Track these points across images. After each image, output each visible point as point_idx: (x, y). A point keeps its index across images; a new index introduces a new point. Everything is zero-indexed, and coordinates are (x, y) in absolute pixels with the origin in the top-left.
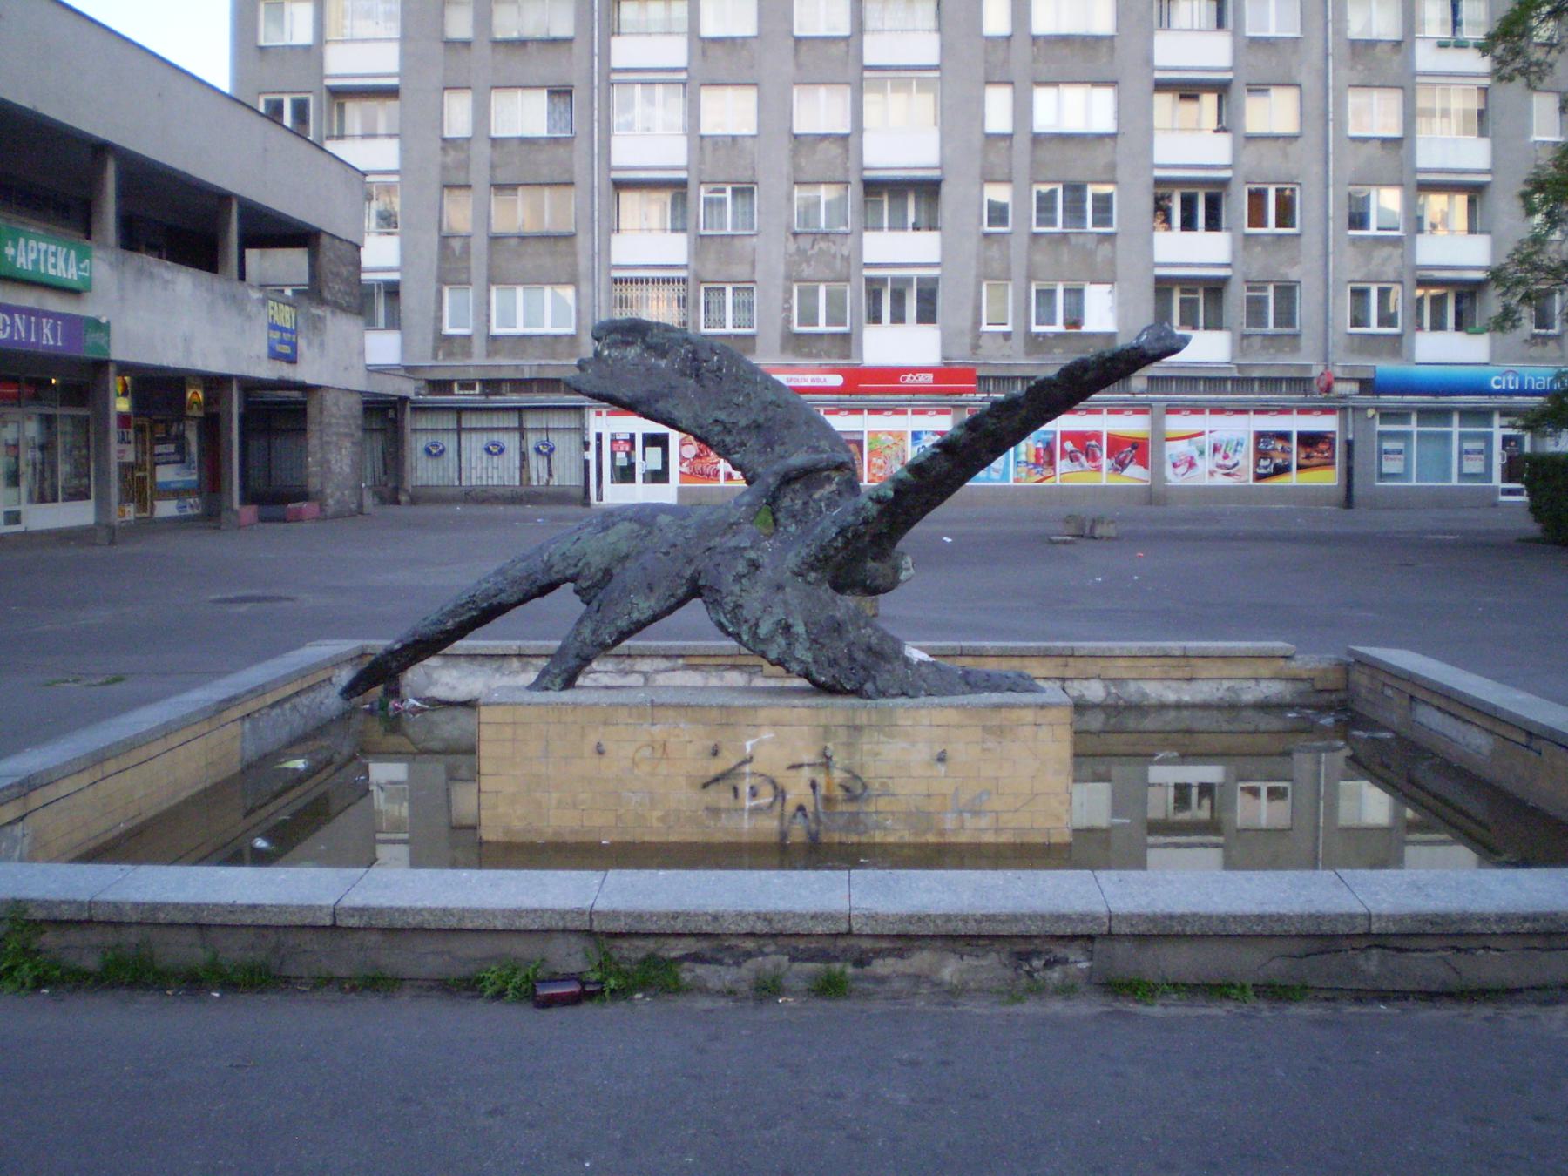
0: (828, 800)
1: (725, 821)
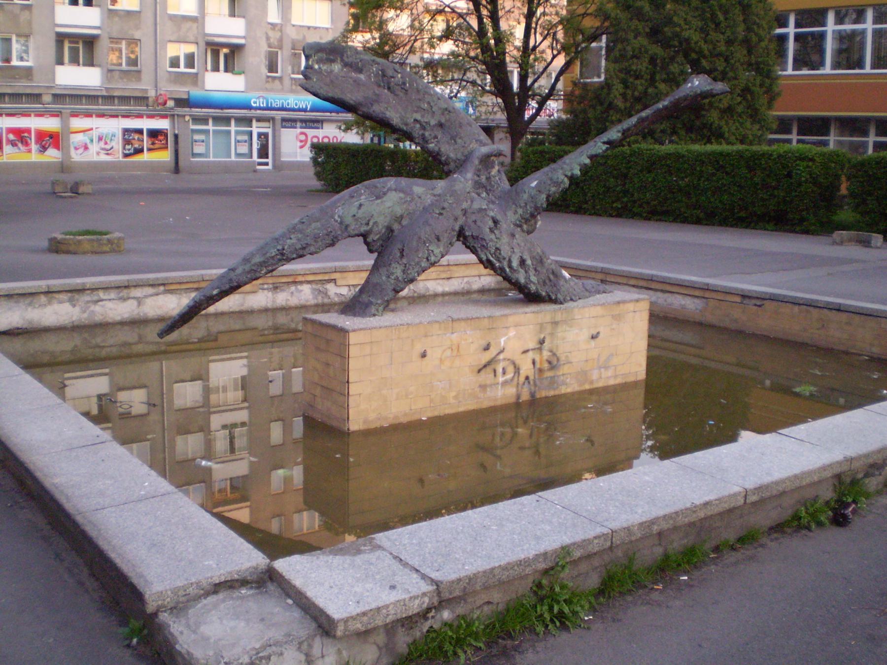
0: (541, 370)
1: (489, 393)
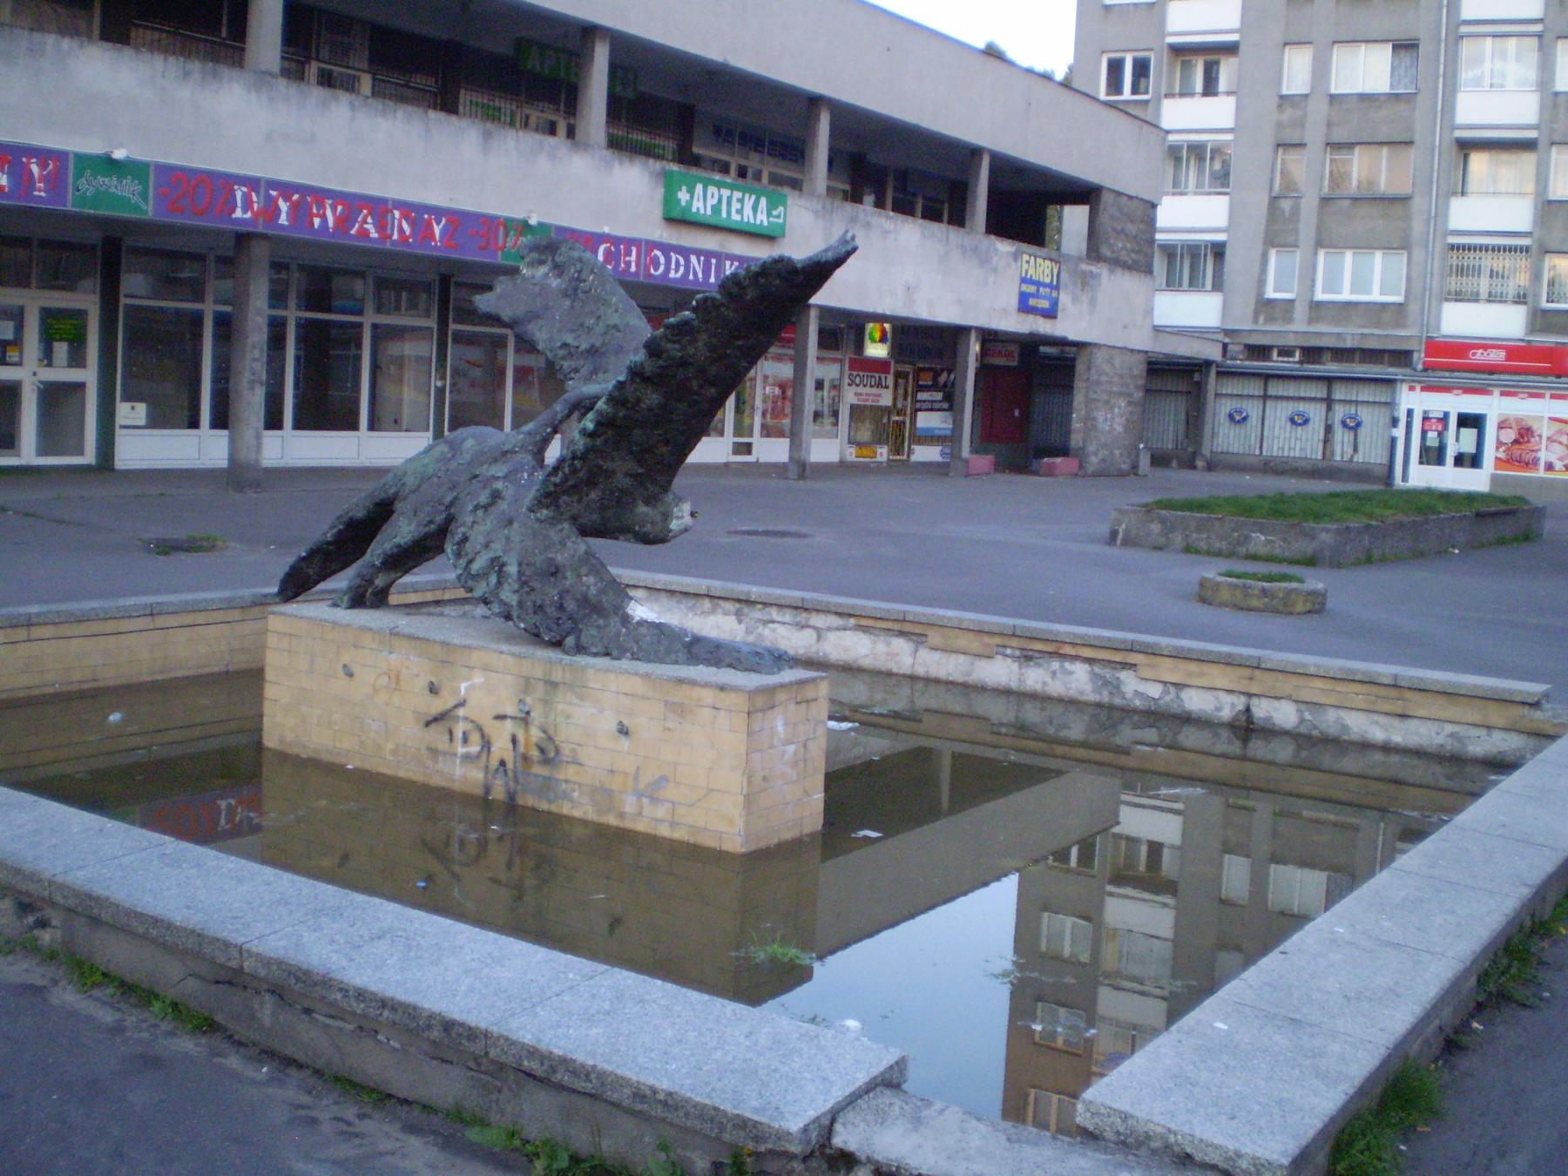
0: (526, 758)
1: (442, 765)
